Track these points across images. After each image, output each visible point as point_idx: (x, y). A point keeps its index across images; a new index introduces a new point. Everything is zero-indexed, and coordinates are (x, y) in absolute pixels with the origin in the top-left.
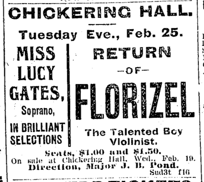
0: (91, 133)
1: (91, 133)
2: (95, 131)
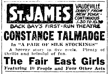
2: (13, 59)
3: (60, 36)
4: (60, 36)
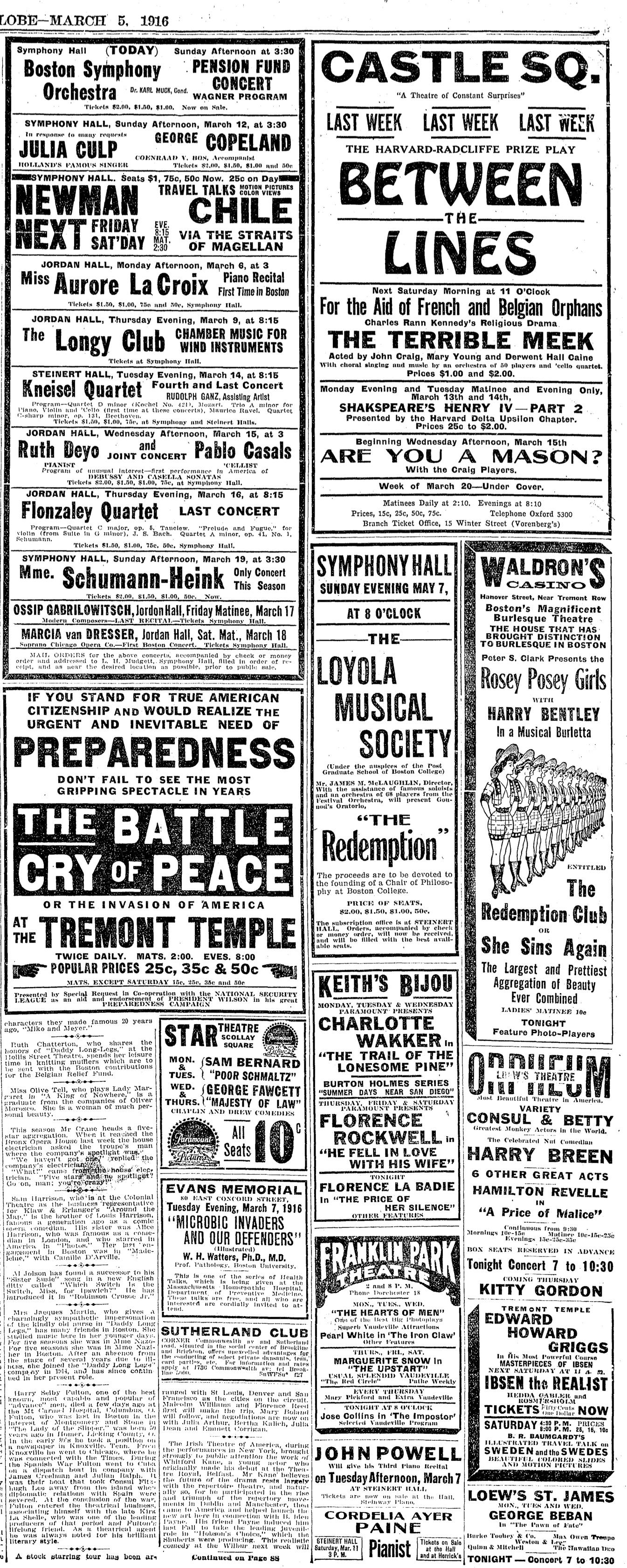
0: (377, 639)
1: (377, 639)
3: (572, 887)
4: (572, 887)
